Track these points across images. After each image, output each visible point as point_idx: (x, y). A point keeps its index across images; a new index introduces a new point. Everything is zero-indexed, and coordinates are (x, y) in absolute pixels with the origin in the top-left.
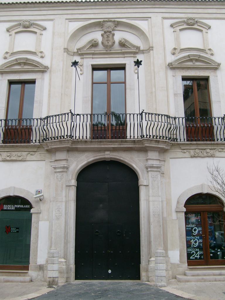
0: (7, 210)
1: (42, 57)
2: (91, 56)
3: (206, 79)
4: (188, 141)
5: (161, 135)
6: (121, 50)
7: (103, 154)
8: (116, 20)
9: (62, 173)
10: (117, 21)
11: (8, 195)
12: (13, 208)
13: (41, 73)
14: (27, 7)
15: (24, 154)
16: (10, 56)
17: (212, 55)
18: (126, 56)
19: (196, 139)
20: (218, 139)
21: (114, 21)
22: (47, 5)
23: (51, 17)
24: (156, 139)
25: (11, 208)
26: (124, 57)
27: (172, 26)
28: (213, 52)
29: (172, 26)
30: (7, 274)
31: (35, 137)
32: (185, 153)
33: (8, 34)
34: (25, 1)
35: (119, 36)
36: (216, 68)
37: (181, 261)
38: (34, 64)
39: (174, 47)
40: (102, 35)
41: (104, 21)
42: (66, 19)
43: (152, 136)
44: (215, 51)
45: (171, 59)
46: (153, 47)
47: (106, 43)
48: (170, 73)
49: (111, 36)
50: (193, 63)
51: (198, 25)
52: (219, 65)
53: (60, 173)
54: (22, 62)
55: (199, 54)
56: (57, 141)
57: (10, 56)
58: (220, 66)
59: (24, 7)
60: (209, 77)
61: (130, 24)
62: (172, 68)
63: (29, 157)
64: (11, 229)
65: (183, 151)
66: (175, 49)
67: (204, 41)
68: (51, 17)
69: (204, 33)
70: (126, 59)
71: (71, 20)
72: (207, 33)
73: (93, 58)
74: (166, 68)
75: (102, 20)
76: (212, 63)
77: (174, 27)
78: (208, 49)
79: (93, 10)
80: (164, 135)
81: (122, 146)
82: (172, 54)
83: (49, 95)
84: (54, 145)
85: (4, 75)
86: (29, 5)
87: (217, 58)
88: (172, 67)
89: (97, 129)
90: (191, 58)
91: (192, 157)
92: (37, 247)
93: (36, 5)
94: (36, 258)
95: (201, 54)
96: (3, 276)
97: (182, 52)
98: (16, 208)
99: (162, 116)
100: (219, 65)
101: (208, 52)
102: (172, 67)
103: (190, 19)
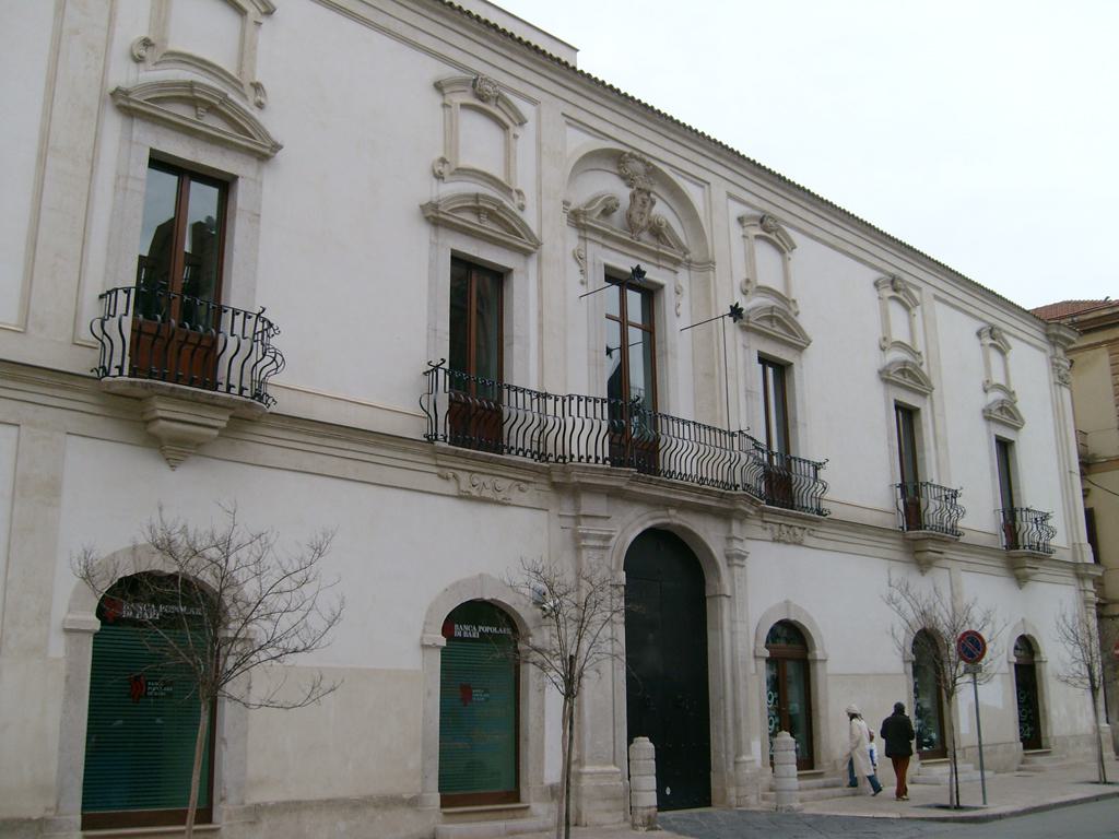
0: (462, 639)
1: (260, 105)
2: (599, 239)
3: (499, 276)
4: (135, 376)
5: (592, 452)
6: (658, 247)
7: (663, 513)
8: (653, 162)
9: (601, 552)
10: (654, 166)
11: (477, 596)
12: (476, 635)
13: (255, 160)
14: (486, 36)
15: (503, 484)
16: (452, 174)
17: (260, 105)
18: (661, 263)
19: (164, 374)
20: (229, 387)
21: (649, 164)
22: (532, 55)
23: (534, 94)
24: (228, 395)
25: (135, 613)
26: (659, 266)
27: (741, 220)
28: (263, 100)
29: (741, 220)
30: (488, 815)
31: (121, 355)
32: (765, 529)
33: (437, 100)
34: (531, 41)
35: (662, 210)
36: (263, 152)
37: (763, 765)
38: (513, 224)
39: (144, 34)
40: (633, 196)
41: (631, 155)
42: (563, 114)
43: (576, 455)
44: (271, 100)
45: (124, 75)
46: (714, 263)
47: (636, 218)
48: (113, 123)
49: (648, 203)
50: (197, 116)
51: (777, 236)
52: (277, 147)
53: (596, 551)
54: (485, 209)
55: (501, 199)
56: (601, 469)
57: (452, 174)
58: (276, 152)
59: (478, 33)
60: (235, 178)
61: (675, 183)
62: (125, 107)
63: (516, 496)
64: (147, 686)
65: (764, 525)
66: (147, 43)
67: (245, 50)
68: (534, 94)
69: (250, 27)
70: (661, 271)
71: (572, 122)
72: (258, 24)
73: (604, 246)
74: (102, 101)
75: (629, 150)
76: (257, 137)
77: (746, 224)
78: (252, 84)
79: (675, 144)
80: (592, 452)
81: (700, 501)
82: (434, 171)
83: (541, 326)
84: (587, 477)
85: (442, 231)
86: (492, 33)
87: (273, 123)
88: (127, 106)
89: (143, 336)
90: (481, 204)
91: (774, 540)
92: (542, 741)
93: (509, 42)
94: (541, 769)
95: (231, 96)
96: (501, 819)
97: (169, 61)
98: (481, 633)
99: (233, 315)
100: (277, 147)
101: (249, 91)
102: (127, 106)
103: (486, 79)
